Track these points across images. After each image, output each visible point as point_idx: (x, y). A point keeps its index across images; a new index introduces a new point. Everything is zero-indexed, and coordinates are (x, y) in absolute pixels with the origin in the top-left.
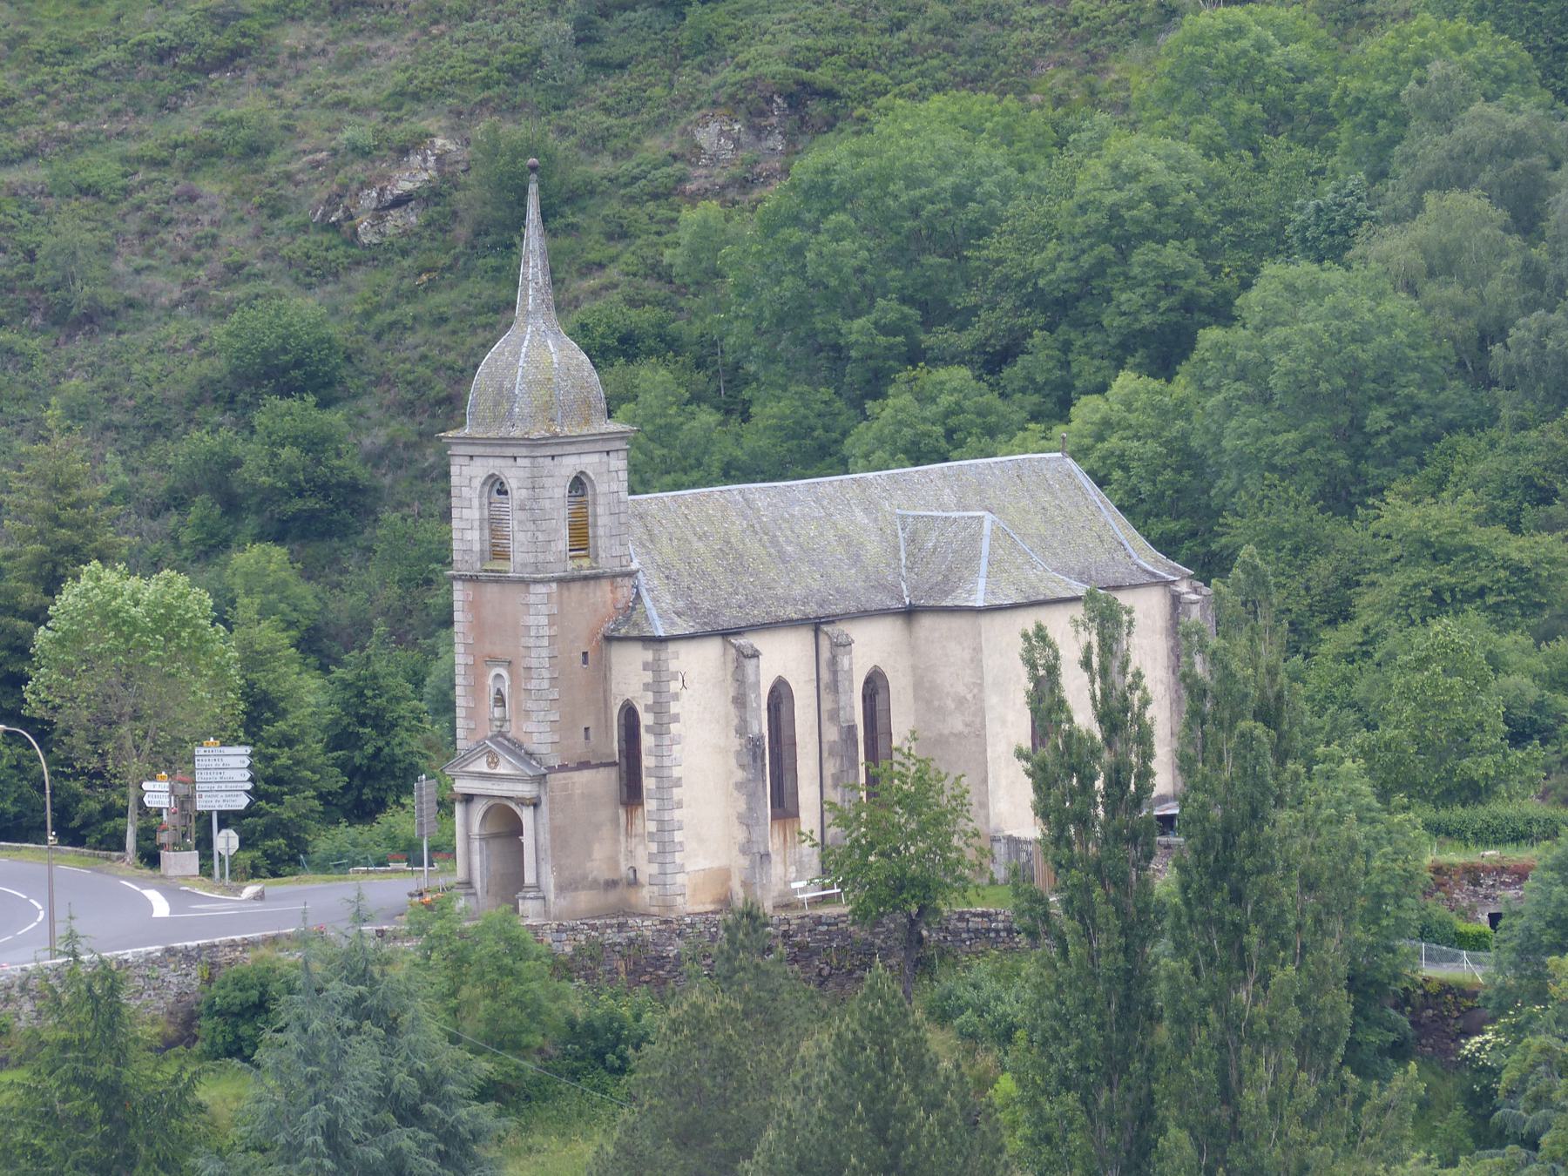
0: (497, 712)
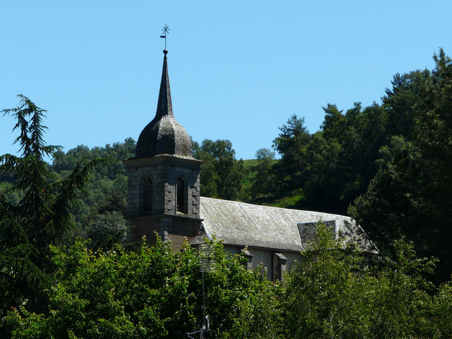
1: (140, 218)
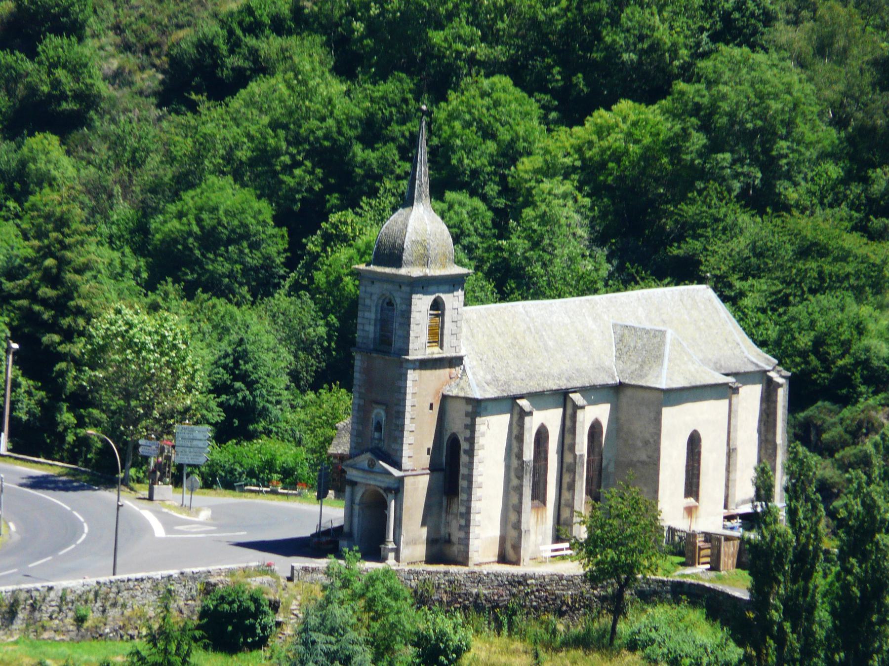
0: (376, 435)
1: (374, 355)
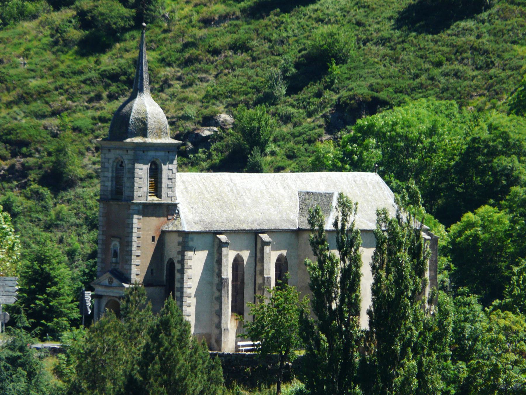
0: (114, 260)
1: (111, 202)
